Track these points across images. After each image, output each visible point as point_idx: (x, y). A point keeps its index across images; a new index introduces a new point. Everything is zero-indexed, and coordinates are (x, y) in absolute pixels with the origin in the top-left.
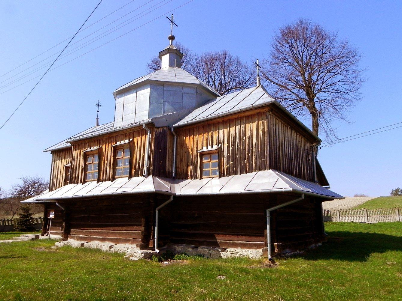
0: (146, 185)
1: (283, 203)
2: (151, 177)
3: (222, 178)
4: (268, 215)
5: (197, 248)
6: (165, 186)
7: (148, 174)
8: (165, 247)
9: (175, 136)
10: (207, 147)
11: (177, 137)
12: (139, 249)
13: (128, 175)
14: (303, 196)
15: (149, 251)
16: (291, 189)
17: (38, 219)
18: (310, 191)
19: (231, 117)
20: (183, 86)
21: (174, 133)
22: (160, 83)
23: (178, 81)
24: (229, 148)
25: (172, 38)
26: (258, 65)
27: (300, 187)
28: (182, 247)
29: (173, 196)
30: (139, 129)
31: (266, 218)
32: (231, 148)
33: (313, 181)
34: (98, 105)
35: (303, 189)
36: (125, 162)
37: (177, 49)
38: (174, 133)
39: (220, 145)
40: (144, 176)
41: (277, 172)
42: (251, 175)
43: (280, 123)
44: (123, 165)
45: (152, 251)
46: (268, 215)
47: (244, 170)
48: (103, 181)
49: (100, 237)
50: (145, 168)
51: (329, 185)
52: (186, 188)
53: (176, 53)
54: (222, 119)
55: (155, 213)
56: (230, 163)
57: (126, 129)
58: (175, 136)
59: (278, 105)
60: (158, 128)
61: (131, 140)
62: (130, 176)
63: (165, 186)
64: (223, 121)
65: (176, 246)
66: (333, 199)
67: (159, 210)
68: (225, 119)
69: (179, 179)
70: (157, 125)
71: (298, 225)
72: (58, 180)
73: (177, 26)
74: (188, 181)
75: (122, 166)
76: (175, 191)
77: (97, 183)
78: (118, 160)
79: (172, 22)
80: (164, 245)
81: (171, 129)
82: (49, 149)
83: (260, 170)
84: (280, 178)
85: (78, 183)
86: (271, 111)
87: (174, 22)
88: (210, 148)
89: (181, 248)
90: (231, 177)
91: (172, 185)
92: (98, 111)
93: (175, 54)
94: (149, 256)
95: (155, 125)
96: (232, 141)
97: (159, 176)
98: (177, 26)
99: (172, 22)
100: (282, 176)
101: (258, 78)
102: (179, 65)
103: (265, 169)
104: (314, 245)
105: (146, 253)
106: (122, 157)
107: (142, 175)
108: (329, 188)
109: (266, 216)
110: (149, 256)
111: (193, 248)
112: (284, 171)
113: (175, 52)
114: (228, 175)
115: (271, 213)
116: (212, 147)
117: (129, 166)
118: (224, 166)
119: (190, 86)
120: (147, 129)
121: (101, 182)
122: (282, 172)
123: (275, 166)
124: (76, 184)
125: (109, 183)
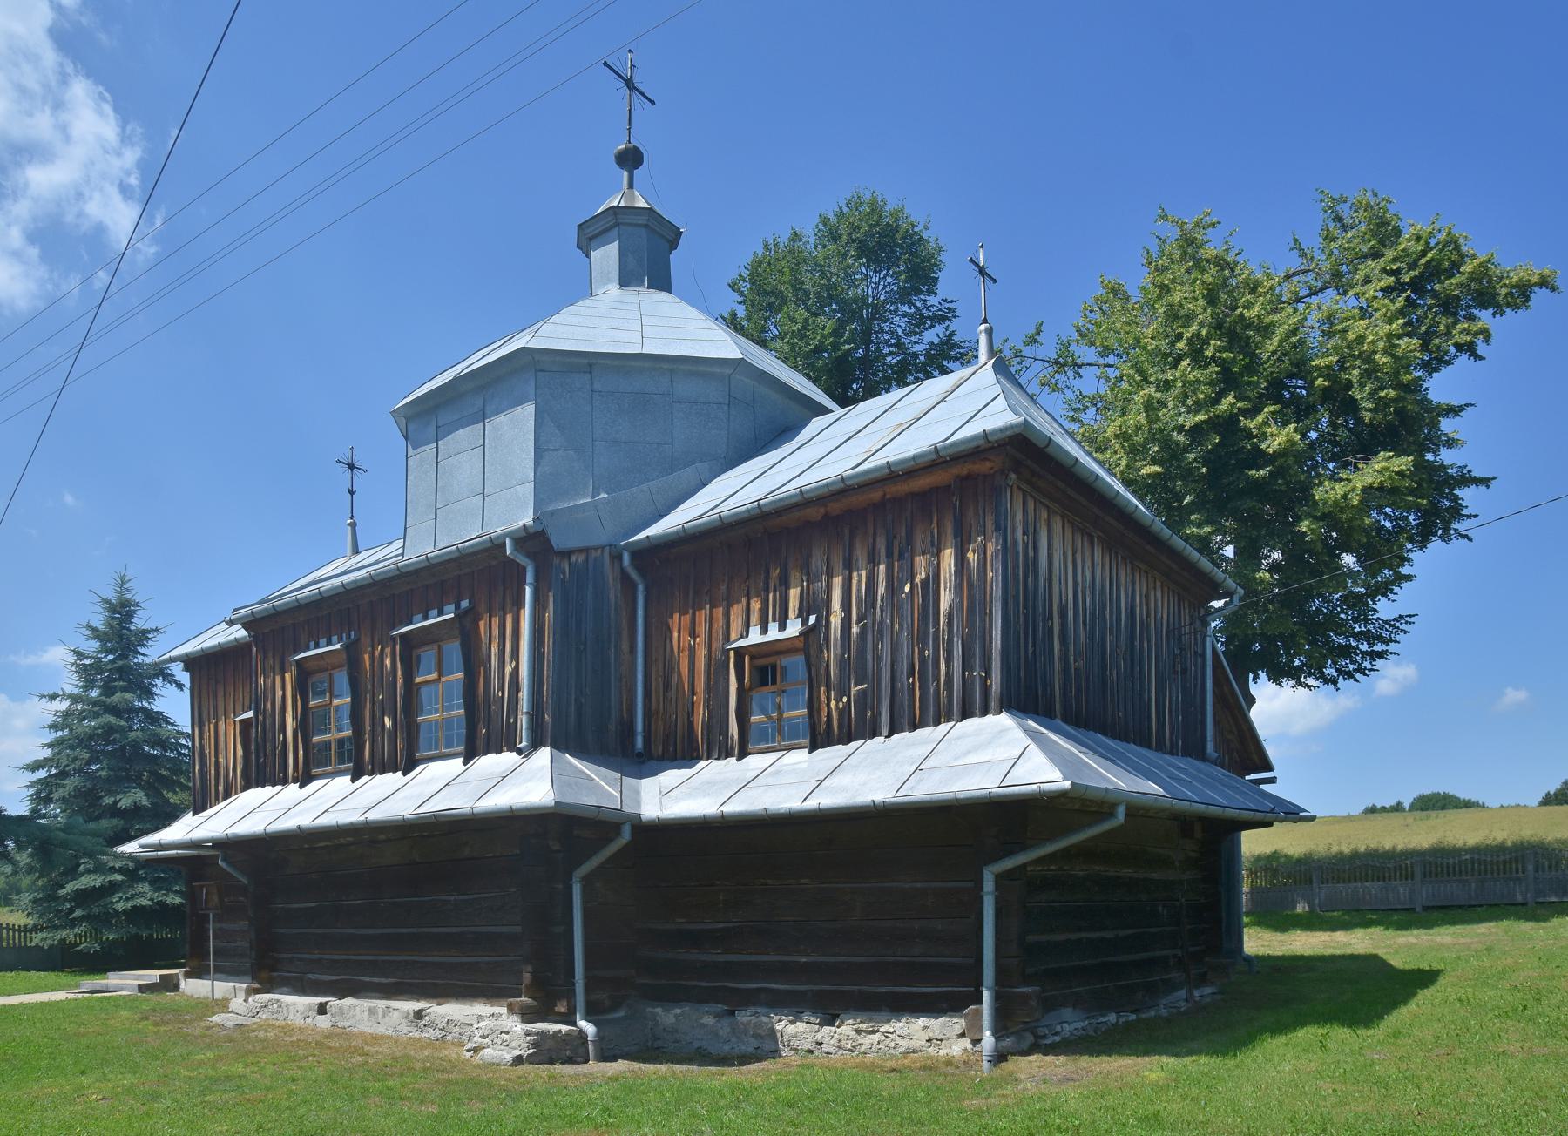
0: (522, 781)
1: (1051, 838)
2: (544, 754)
3: (820, 753)
4: (989, 885)
5: (732, 1013)
6: (599, 787)
7: (536, 744)
8: (621, 1014)
9: (641, 588)
10: (765, 631)
11: (647, 589)
12: (516, 1018)
13: (461, 749)
14: (1121, 812)
15: (553, 1027)
16: (1067, 784)
17: (19, 931)
18: (1160, 790)
19: (856, 500)
20: (671, 371)
21: (633, 574)
22: (717, 370)
23: (650, 349)
24: (850, 628)
25: (630, 159)
26: (982, 271)
27: (1111, 777)
28: (678, 1011)
29: (1127, 808)
30: (494, 563)
31: (981, 898)
32: (855, 630)
33: (1194, 750)
34: (351, 466)
35: (1122, 785)
36: (449, 698)
37: (651, 209)
38: (633, 574)
39: (812, 619)
40: (520, 751)
41: (1031, 723)
42: (927, 735)
43: (1057, 525)
44: (442, 709)
45: (564, 1028)
46: (989, 885)
47: (905, 719)
48: (372, 773)
49: (383, 980)
50: (523, 721)
51: (1269, 768)
52: (678, 795)
53: (646, 226)
54: (822, 510)
55: (570, 888)
56: (854, 690)
57: (441, 563)
58: (641, 588)
59: (1041, 444)
60: (567, 554)
61: (465, 604)
62: (469, 757)
63: (599, 787)
64: (826, 515)
65: (659, 1010)
66: (1270, 824)
67: (587, 881)
68: (835, 507)
69: (661, 758)
70: (559, 541)
71: (1129, 923)
72: (222, 771)
73: (653, 103)
74: (702, 764)
75: (437, 711)
76: (639, 804)
77: (353, 781)
78: (424, 691)
79: (629, 84)
80: (614, 1007)
81: (620, 558)
82: (173, 654)
83: (965, 714)
84: (1033, 746)
85: (285, 782)
86: (1016, 472)
87: (623, 84)
88: (774, 634)
89: (676, 1016)
90: (854, 745)
91: (628, 781)
92: (352, 492)
93: (643, 231)
94: (569, 1051)
95: (554, 541)
96: (859, 597)
97: (582, 752)
98: (653, 103)
99: (629, 84)
100: (1052, 736)
101: (983, 327)
102: (662, 282)
103: (984, 713)
104: (1182, 993)
105: (543, 1035)
106: (435, 676)
107: (513, 748)
108: (1272, 781)
109: (981, 888)
110: (547, 1052)
111: (718, 1016)
112: (1066, 720)
113: (642, 220)
114: (846, 739)
115: (999, 878)
116: (782, 627)
117: (462, 711)
118: (828, 705)
119: (701, 369)
120: (522, 560)
121: (366, 778)
122: (1058, 721)
123: (1027, 699)
124: (279, 787)
125: (393, 779)
